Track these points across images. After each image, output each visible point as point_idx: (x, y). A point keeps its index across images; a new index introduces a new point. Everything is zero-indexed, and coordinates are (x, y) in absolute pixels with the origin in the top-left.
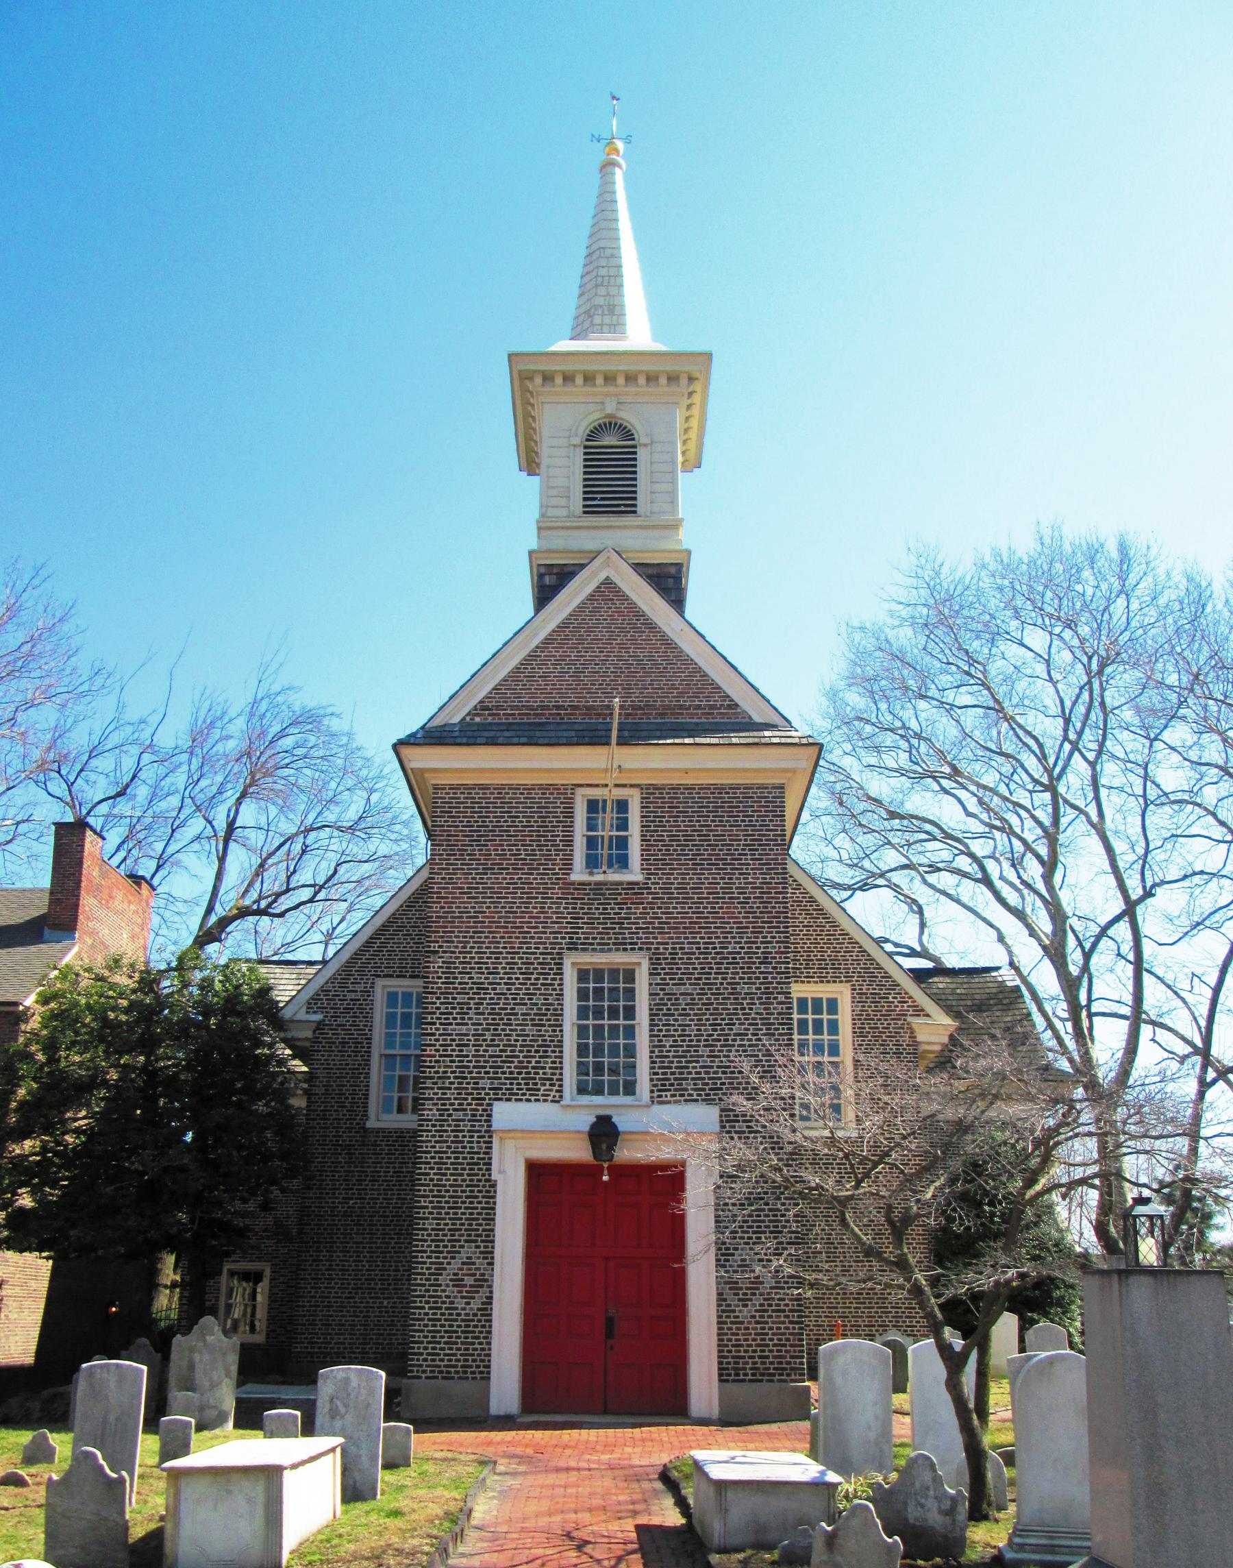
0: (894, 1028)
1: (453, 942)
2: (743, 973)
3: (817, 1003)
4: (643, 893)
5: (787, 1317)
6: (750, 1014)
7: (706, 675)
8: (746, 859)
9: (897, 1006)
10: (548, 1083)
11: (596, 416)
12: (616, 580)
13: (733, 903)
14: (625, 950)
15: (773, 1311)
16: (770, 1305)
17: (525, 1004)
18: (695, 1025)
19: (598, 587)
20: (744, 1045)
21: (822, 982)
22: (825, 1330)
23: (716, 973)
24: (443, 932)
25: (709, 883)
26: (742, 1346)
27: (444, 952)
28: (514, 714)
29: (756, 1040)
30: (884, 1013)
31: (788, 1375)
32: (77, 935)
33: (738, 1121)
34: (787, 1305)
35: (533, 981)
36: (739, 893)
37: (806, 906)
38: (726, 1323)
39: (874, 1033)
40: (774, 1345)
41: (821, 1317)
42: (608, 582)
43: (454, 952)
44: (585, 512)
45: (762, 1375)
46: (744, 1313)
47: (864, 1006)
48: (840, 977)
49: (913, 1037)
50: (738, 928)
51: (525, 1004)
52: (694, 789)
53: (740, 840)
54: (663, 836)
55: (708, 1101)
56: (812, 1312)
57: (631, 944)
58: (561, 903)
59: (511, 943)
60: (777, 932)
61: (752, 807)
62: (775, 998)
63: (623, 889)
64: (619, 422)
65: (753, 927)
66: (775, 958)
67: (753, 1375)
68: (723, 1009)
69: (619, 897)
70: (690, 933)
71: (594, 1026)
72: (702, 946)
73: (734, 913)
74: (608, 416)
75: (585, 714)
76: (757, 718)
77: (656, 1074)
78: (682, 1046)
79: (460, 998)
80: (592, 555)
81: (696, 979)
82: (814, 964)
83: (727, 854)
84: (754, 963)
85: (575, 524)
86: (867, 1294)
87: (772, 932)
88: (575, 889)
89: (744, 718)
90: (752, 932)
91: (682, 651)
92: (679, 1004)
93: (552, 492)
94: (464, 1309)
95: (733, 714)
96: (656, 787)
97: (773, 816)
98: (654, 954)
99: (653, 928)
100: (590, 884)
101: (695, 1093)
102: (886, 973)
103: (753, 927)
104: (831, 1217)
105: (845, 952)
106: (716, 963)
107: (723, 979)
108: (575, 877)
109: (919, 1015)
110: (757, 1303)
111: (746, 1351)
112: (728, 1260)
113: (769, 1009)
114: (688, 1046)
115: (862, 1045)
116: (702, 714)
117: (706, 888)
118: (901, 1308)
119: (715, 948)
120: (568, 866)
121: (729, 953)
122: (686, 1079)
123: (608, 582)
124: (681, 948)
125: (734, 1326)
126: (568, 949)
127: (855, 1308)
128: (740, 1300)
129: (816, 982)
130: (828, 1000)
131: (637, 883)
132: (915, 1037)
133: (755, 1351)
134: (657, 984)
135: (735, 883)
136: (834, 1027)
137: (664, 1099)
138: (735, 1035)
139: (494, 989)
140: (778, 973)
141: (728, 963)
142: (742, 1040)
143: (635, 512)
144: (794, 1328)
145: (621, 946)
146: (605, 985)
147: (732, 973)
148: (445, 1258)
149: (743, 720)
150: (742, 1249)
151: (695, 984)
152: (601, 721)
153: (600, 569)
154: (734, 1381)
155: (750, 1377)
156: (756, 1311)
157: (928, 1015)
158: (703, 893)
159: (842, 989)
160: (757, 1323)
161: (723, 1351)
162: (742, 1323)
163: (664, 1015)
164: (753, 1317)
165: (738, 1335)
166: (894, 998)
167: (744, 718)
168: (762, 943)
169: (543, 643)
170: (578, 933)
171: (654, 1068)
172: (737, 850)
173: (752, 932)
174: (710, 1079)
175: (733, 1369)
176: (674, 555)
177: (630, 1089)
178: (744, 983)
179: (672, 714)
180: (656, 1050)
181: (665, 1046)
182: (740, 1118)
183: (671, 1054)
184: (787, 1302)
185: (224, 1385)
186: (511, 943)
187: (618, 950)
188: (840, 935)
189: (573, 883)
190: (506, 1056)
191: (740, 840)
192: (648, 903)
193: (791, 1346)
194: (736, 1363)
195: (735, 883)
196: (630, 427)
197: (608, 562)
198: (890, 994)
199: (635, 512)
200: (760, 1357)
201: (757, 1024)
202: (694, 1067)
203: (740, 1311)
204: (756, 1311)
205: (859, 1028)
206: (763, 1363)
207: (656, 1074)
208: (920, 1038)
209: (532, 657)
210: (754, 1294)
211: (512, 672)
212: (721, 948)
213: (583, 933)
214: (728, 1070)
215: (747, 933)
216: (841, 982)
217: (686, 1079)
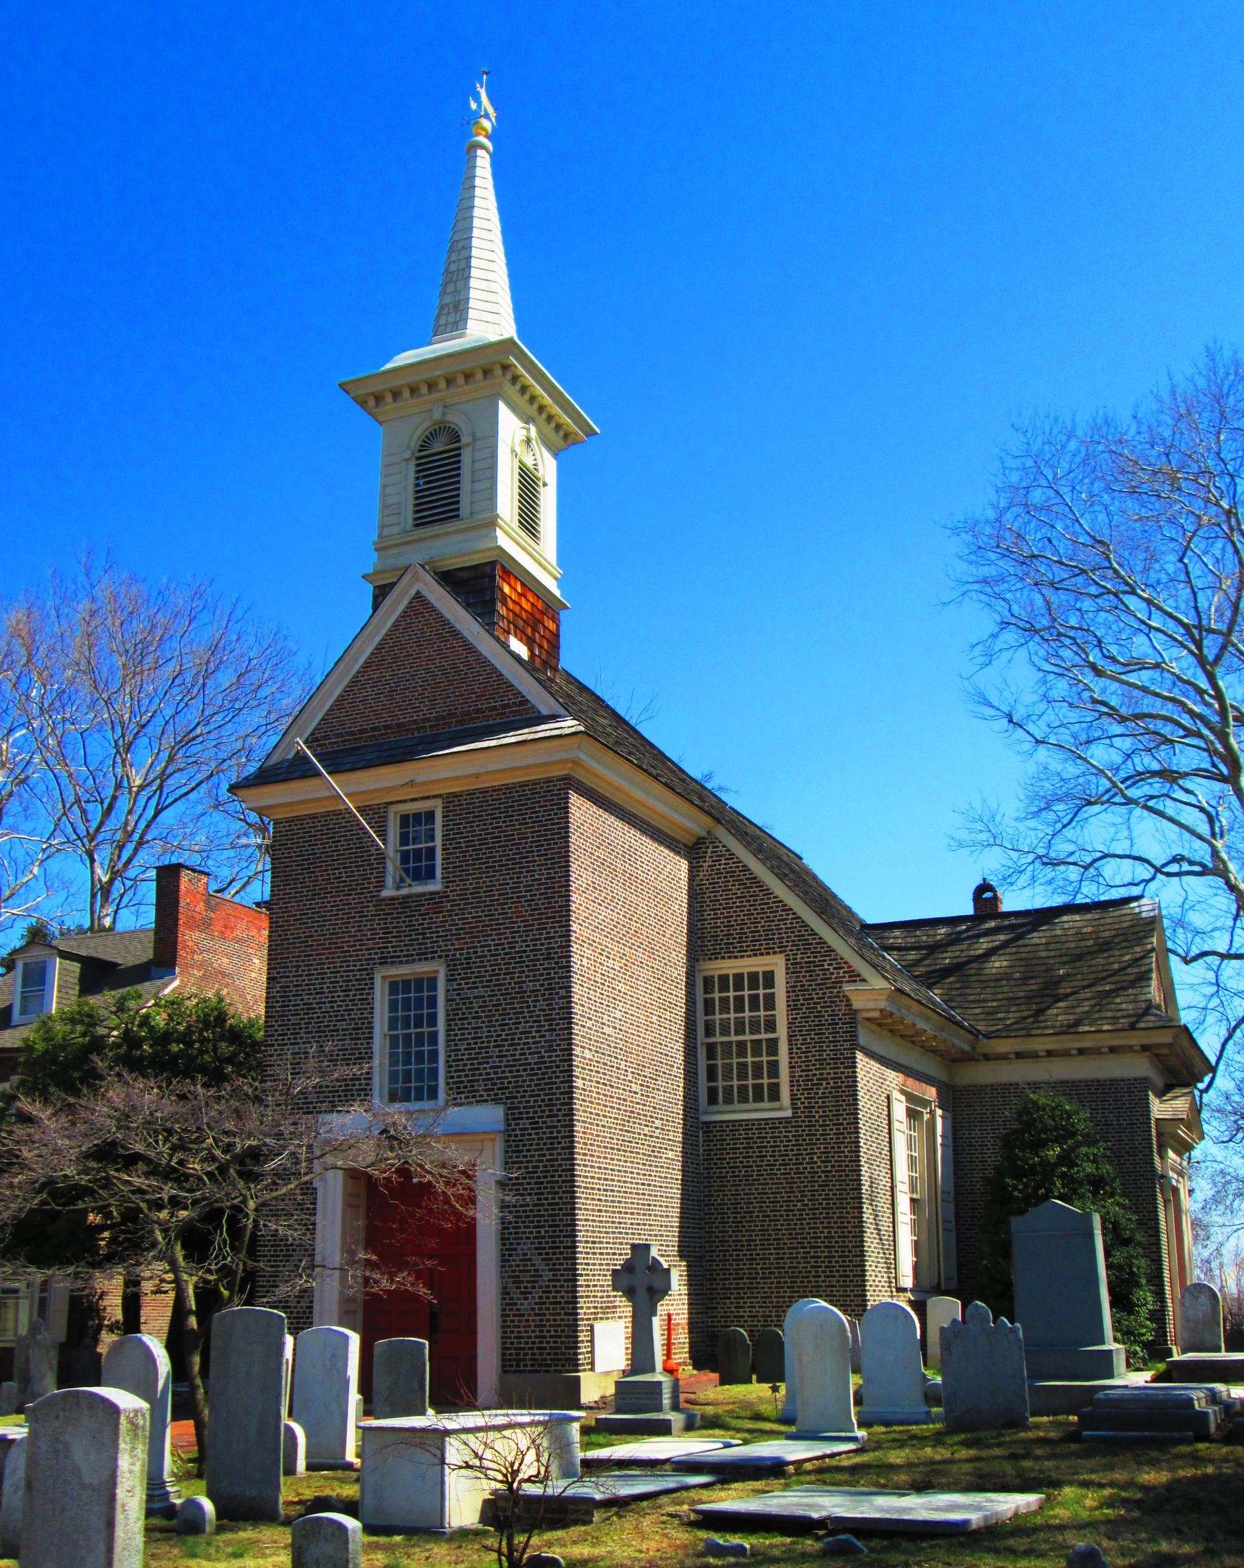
0: (829, 997)
1: (287, 967)
2: (529, 971)
3: (753, 977)
4: (442, 902)
5: (563, 1308)
6: (534, 1011)
7: (502, 675)
8: (533, 856)
9: (833, 974)
10: (362, 1093)
11: (425, 425)
12: (425, 593)
13: (521, 902)
14: (426, 959)
15: (551, 1303)
16: (548, 1298)
17: (345, 1020)
18: (487, 1027)
19: (411, 603)
20: (528, 1043)
21: (755, 955)
22: (759, 1321)
23: (505, 974)
24: (281, 959)
25: (500, 885)
26: (522, 1337)
27: (281, 977)
28: (337, 742)
29: (540, 1037)
30: (819, 982)
31: (563, 1365)
32: (177, 970)
33: (522, 1119)
34: (562, 1297)
35: (351, 998)
36: (526, 891)
37: (739, 876)
38: (509, 1316)
39: (809, 1004)
40: (551, 1337)
41: (755, 1307)
42: (418, 596)
43: (289, 977)
44: (417, 525)
45: (540, 1365)
46: (524, 1305)
47: (798, 977)
48: (773, 948)
49: (849, 1005)
50: (525, 926)
51: (345, 1020)
52: (488, 792)
53: (528, 838)
54: (460, 843)
55: (497, 1101)
56: (746, 1303)
57: (432, 953)
58: (374, 920)
59: (333, 963)
60: (560, 927)
61: (539, 802)
62: (557, 993)
63: (426, 900)
64: (448, 425)
65: (539, 924)
66: (557, 953)
67: (532, 1365)
68: (510, 1009)
69: (423, 908)
70: (483, 936)
71: (416, 1034)
72: (493, 948)
73: (521, 912)
74: (436, 423)
75: (397, 732)
76: (545, 712)
77: (452, 1077)
78: (474, 1049)
79: (294, 1019)
80: (401, 572)
81: (487, 981)
82: (747, 937)
83: (516, 854)
84: (539, 960)
85: (403, 540)
86: (801, 1282)
87: (555, 927)
88: (386, 905)
89: (534, 712)
90: (537, 929)
91: (481, 654)
92: (473, 1008)
93: (387, 512)
94: (295, 1307)
95: (524, 710)
96: (455, 795)
97: (558, 809)
98: (451, 960)
99: (451, 935)
100: (398, 899)
101: (485, 1093)
102: (820, 938)
103: (539, 924)
104: (765, 1202)
105: (779, 920)
106: (505, 964)
107: (511, 978)
108: (385, 893)
109: (855, 981)
110: (537, 1296)
111: (526, 1343)
112: (511, 1255)
113: (551, 1004)
114: (480, 1048)
115: (796, 1019)
116: (497, 715)
117: (497, 890)
118: (835, 1296)
119: (504, 949)
120: (381, 884)
121: (517, 952)
122: (478, 1081)
123: (418, 596)
124: (475, 953)
125: (516, 1319)
126: (380, 964)
127: (789, 1297)
128: (522, 1293)
129: (749, 956)
130: (764, 973)
131: (437, 893)
132: (851, 1005)
133: (534, 1343)
134: (454, 990)
135: (522, 882)
136: (770, 1002)
137: (458, 1101)
138: (522, 1033)
139: (320, 1008)
140: (560, 968)
141: (515, 963)
142: (527, 1038)
143: (458, 516)
144: (569, 1320)
145: (424, 956)
146: (412, 995)
147: (519, 972)
148: (281, 1261)
149: (534, 715)
150: (524, 1244)
151: (487, 986)
152: (410, 736)
153: (411, 585)
154: (515, 1372)
155: (529, 1368)
156: (536, 1303)
157: (864, 980)
158: (494, 895)
159: (775, 961)
160: (536, 1315)
161: (506, 1343)
162: (523, 1315)
163: (460, 1019)
164: (533, 1309)
165: (519, 1327)
166: (829, 965)
167: (534, 712)
168: (546, 939)
169: (364, 668)
170: (387, 947)
171: (450, 1072)
172: (525, 848)
173: (537, 929)
174: (498, 1079)
175: (515, 1360)
176: (489, 554)
177: (433, 1094)
178: (530, 981)
179: (470, 719)
180: (453, 1054)
181: (460, 1050)
182: (524, 1116)
183: (465, 1057)
184: (563, 1294)
185: (48, 1375)
186: (333, 963)
187: (420, 960)
188: (774, 902)
189: (384, 899)
190: (482, 1058)
191: (528, 838)
192: (447, 911)
193: (566, 1337)
194: (518, 1354)
195: (522, 882)
196: (457, 429)
197: (416, 578)
198: (825, 961)
199: (458, 516)
200: (539, 1348)
201: (540, 1021)
202: (485, 1069)
203: (521, 1304)
204: (536, 1303)
205: (793, 1001)
206: (541, 1354)
207: (452, 1077)
208: (856, 1005)
209: (354, 682)
210: (533, 1287)
211: (337, 700)
212: (509, 948)
213: (392, 947)
214: (514, 1069)
215: (532, 930)
216: (775, 953)
217: (478, 1081)
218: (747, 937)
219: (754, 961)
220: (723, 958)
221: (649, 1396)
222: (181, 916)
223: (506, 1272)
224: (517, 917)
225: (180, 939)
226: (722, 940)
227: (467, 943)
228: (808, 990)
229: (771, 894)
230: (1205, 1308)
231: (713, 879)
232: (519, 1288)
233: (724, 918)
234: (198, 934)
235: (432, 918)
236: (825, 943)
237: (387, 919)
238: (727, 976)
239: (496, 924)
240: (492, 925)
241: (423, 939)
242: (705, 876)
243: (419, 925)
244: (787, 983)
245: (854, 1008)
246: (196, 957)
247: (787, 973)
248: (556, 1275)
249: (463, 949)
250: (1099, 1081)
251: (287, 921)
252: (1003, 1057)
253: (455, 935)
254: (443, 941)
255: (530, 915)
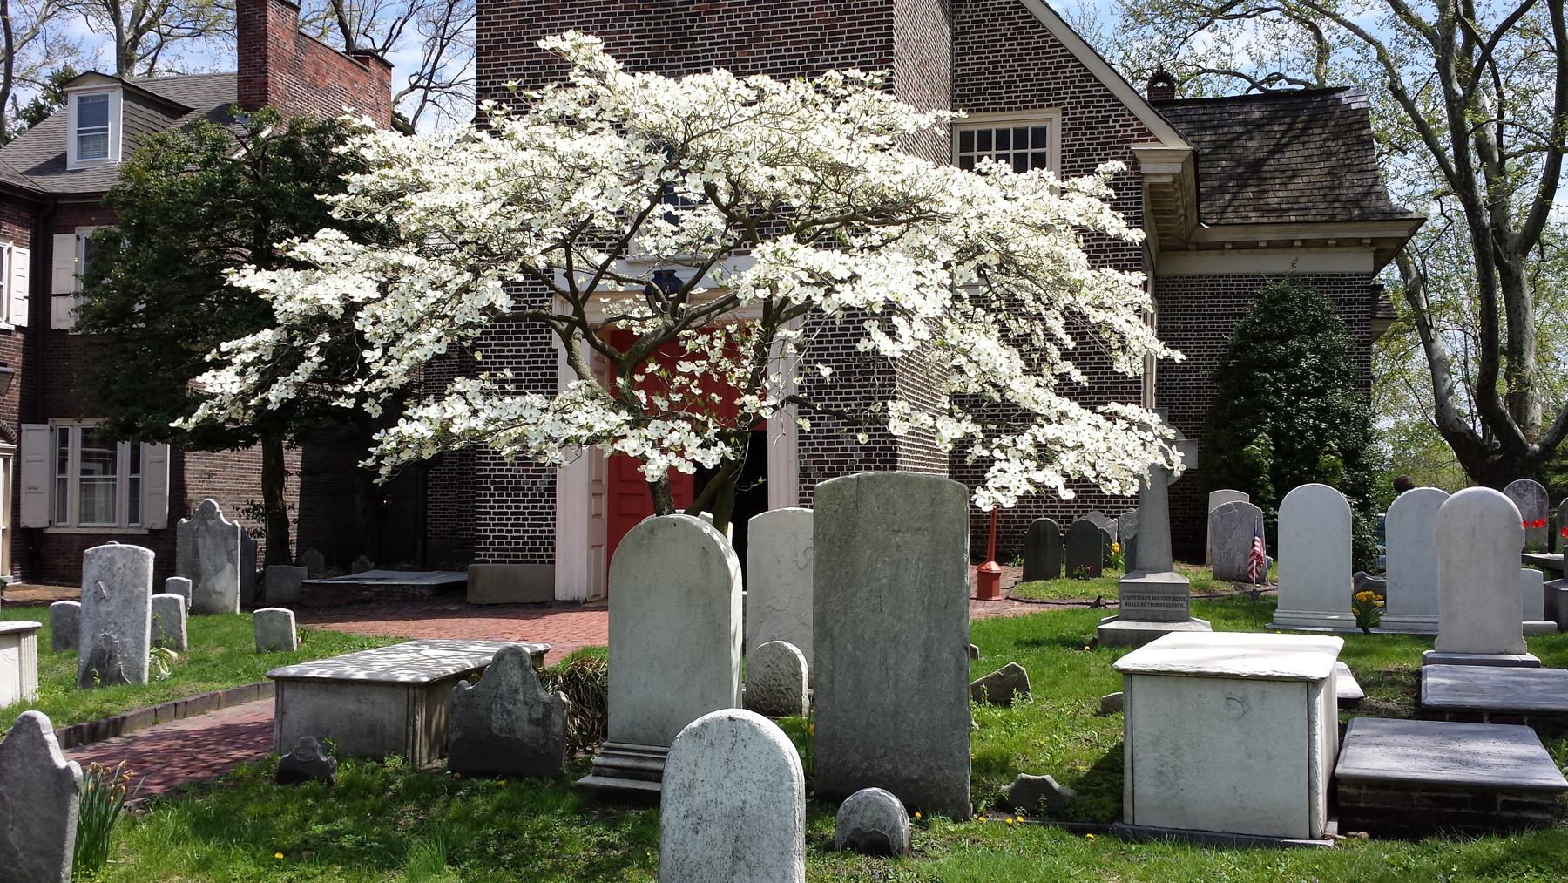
3: (1021, 135)
47: (1077, 134)
50: (830, 34)
65: (849, 32)
70: (774, 45)
94: (529, 489)
99: (730, 42)
103: (849, 32)
129: (1019, 109)
159: (1049, 116)
170: (644, 55)
215: (842, 39)
218: (1018, 86)
219: (1013, 115)
220: (987, 110)
221: (1170, 602)
222: (270, 53)
223: (805, 450)
224: (820, 21)
225: (270, 80)
226: (986, 89)
227: (753, 53)
228: (1088, 150)
229: (1049, 36)
230: (1529, 508)
231: (978, 16)
232: (823, 469)
233: (990, 63)
234: (288, 76)
235: (704, 20)
236: (1112, 95)
237: (642, 19)
238: (990, 132)
239: (792, 30)
240: (786, 31)
241: (692, 46)
242: (967, 12)
243: (686, 28)
244: (1063, 141)
245: (1143, 171)
246: (287, 103)
247: (1063, 130)
248: (871, 455)
249: (747, 60)
250: (1317, 275)
251: (502, 17)
252: (1220, 247)
253: (736, 42)
254: (719, 50)
255: (838, 20)
